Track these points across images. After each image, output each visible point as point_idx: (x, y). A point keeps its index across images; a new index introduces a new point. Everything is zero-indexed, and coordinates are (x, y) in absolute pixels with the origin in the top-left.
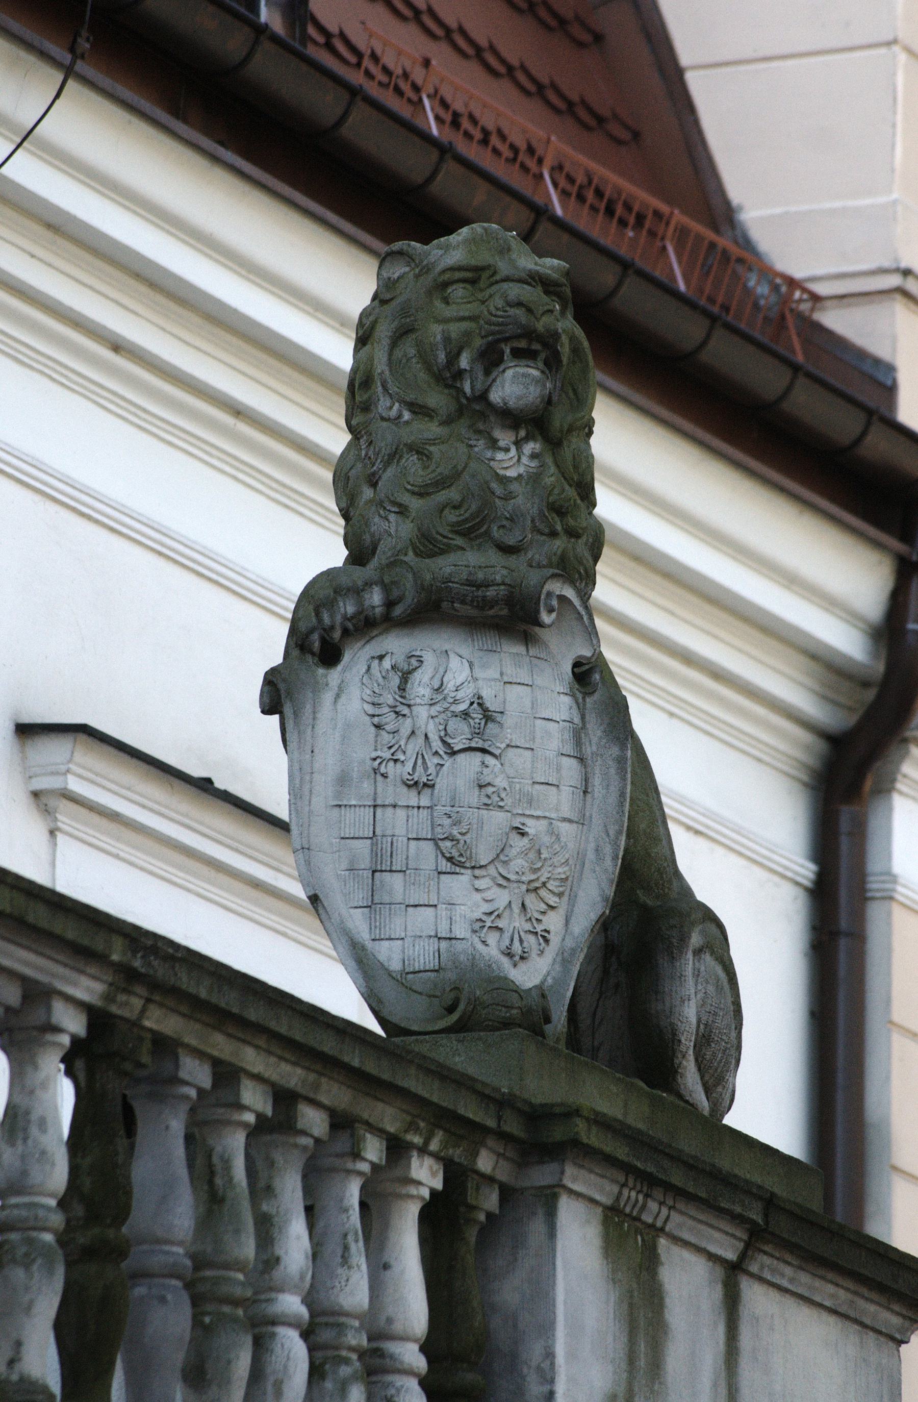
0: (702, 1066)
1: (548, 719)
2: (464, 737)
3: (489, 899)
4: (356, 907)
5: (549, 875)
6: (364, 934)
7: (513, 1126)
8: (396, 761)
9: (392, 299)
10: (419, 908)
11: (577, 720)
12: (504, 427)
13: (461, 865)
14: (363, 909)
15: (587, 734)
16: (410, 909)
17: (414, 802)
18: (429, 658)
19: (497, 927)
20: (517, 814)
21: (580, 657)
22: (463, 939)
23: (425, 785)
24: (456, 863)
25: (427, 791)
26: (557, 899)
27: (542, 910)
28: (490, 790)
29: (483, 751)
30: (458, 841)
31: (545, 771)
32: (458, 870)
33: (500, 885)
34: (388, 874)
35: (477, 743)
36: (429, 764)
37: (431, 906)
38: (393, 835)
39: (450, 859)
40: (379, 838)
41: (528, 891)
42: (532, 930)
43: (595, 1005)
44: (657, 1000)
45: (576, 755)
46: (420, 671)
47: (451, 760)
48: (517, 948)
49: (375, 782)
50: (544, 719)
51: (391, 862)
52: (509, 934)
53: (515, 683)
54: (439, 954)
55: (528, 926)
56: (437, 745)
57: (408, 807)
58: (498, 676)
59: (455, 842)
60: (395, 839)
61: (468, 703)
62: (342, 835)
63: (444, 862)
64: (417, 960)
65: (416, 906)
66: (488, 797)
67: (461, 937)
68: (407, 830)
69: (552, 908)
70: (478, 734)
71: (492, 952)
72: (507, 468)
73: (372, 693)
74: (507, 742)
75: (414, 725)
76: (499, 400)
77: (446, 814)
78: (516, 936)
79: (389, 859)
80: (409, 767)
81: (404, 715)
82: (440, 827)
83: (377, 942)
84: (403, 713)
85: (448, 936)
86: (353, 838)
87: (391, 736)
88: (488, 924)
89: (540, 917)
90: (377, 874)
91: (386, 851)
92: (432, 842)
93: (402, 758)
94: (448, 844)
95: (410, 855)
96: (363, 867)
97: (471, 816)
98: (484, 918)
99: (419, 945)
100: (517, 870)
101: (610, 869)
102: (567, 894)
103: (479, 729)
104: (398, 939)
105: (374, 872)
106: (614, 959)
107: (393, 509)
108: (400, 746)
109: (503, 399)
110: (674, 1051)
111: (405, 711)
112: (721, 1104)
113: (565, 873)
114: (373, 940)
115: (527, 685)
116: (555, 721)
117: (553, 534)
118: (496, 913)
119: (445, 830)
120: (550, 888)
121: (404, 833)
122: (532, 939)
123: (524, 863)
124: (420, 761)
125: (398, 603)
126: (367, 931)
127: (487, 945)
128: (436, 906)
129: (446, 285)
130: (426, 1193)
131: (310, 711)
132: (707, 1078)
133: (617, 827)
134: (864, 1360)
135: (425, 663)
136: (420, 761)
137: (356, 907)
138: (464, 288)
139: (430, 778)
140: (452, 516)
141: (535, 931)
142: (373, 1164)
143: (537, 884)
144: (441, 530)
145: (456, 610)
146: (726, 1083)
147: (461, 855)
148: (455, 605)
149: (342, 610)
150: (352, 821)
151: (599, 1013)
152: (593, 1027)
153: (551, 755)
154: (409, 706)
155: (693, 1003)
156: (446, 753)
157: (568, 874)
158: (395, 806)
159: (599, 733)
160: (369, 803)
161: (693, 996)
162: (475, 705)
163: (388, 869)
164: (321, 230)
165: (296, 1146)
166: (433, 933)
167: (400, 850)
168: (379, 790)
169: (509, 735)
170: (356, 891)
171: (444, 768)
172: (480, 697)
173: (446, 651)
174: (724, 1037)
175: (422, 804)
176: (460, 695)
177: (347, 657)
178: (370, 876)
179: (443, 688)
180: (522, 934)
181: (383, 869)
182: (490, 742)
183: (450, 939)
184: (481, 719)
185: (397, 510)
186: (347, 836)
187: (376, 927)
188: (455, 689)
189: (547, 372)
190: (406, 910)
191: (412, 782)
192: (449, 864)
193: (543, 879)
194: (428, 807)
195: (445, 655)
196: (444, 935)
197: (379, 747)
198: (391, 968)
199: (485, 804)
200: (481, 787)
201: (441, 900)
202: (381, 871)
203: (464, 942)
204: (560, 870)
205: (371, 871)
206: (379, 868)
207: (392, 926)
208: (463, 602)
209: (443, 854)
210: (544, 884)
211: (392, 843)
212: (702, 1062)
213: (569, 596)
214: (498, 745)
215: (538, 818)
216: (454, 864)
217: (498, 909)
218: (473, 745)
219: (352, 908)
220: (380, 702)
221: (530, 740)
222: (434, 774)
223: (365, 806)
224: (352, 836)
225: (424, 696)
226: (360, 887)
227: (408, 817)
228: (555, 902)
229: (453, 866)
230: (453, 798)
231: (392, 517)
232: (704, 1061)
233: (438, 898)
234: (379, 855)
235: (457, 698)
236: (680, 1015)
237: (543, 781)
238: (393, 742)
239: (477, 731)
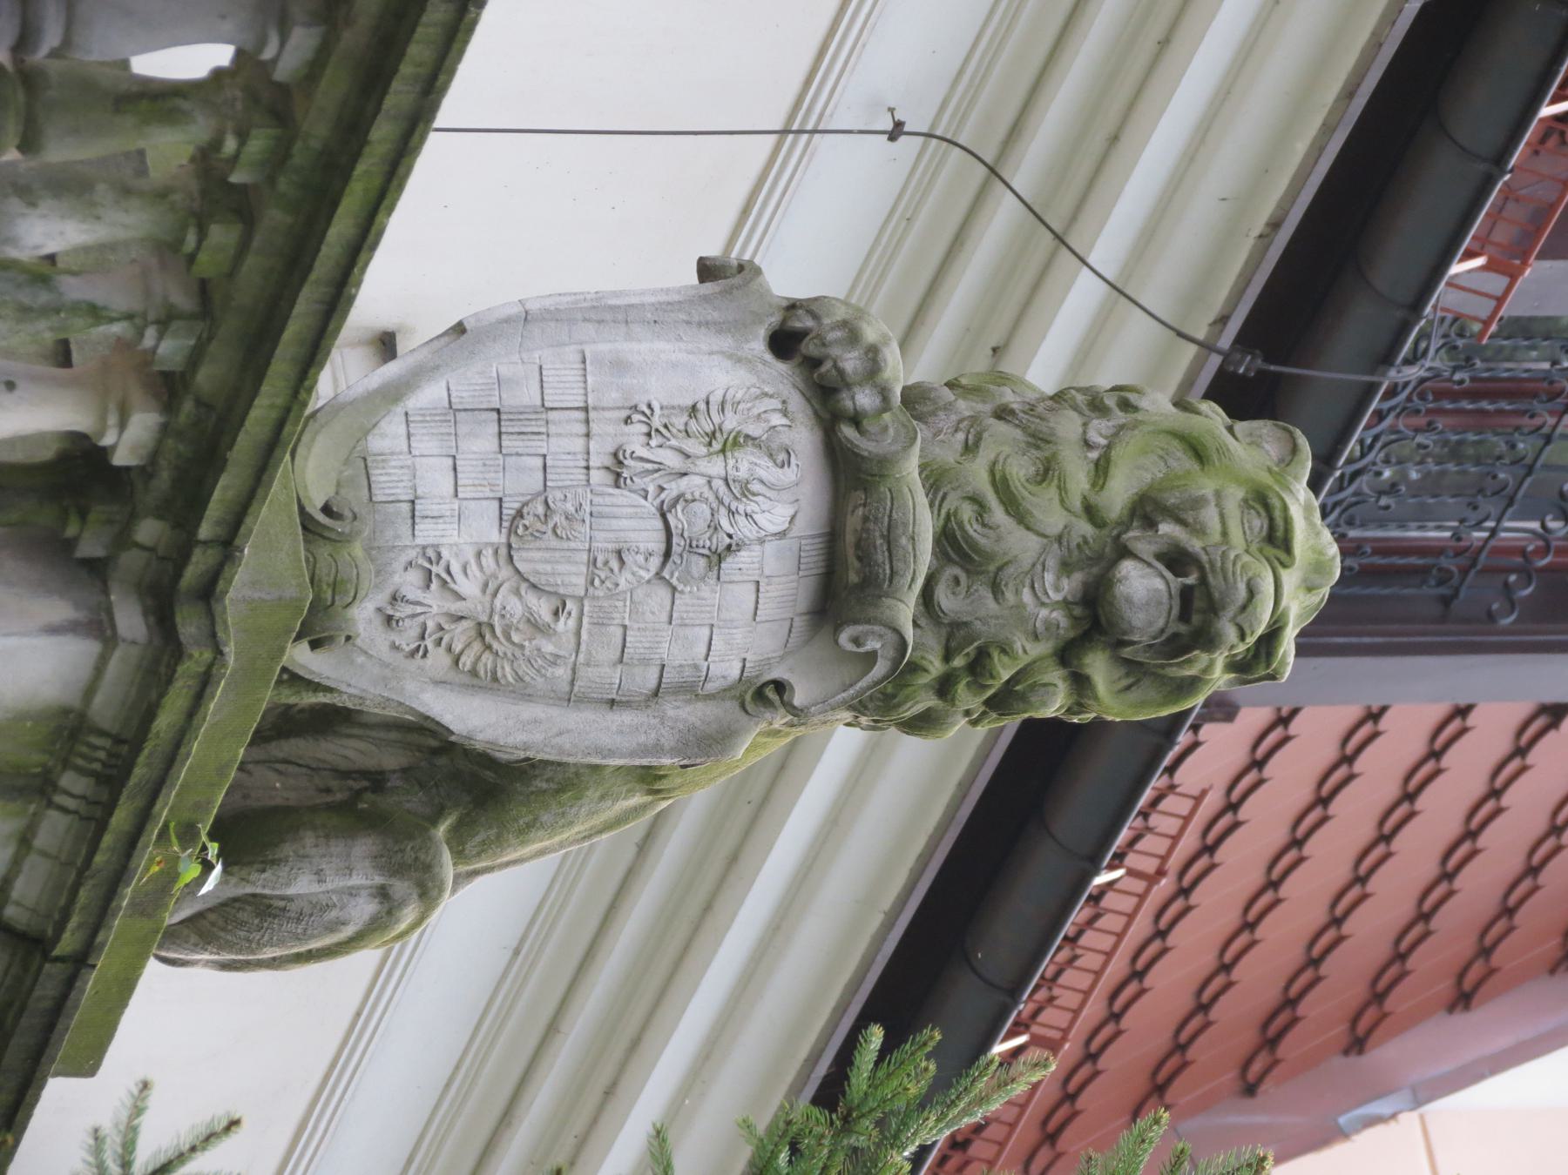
0: (228, 909)
1: (710, 644)
2: (686, 526)
3: (469, 571)
4: (449, 390)
5: (500, 654)
6: (415, 402)
8: (649, 435)
9: (1236, 439)
10: (452, 473)
11: (711, 687)
12: (1086, 585)
13: (512, 530)
14: (447, 399)
15: (688, 702)
16: (450, 461)
17: (595, 462)
18: (789, 475)
19: (430, 580)
20: (583, 605)
21: (792, 689)
22: (414, 535)
23: (618, 475)
24: (516, 522)
25: (610, 478)
26: (468, 667)
27: (453, 646)
28: (615, 564)
29: (667, 554)
30: (546, 522)
31: (641, 642)
32: (506, 524)
33: (486, 585)
34: (496, 429)
35: (679, 545)
36: (647, 480)
37: (456, 491)
38: (548, 435)
39: (520, 514)
40: (544, 416)
41: (480, 624)
42: (427, 633)
43: (301, 762)
44: (318, 837)
45: (663, 686)
46: (770, 464)
47: (653, 510)
48: (403, 611)
49: (619, 408)
50: (711, 639)
51: (512, 433)
52: (421, 600)
53: (758, 597)
54: (392, 502)
55: (431, 625)
57: (588, 453)
58: (767, 572)
59: (542, 518)
60: (544, 437)
61: (731, 531)
62: (544, 367)
63: (517, 505)
64: (383, 471)
65: (455, 469)
66: (606, 563)
67: (416, 533)
68: (557, 453)
69: (457, 662)
70: (691, 546)
71: (398, 575)
72: (1033, 587)
73: (736, 400)
74: (680, 587)
75: (698, 457)
76: (1124, 572)
77: (581, 505)
78: (419, 609)
79: (516, 429)
80: (642, 452)
81: (710, 444)
82: (563, 498)
83: (404, 418)
84: (714, 442)
85: (417, 513)
86: (542, 380)
87: (682, 428)
88: (434, 569)
89: (444, 643)
90: (494, 415)
91: (525, 426)
92: (542, 488)
93: (653, 443)
94: (540, 510)
95: (524, 458)
96: (504, 396)
98: (443, 563)
99: (403, 474)
100: (508, 608)
101: (510, 740)
102: (475, 681)
103: (697, 546)
104: (410, 446)
105: (498, 411)
106: (365, 783)
107: (970, 437)
108: (669, 440)
109: (1126, 578)
110: (251, 863)
111: (717, 446)
112: (174, 943)
113: (504, 676)
114: (406, 414)
115: (755, 614)
116: (708, 655)
117: (947, 658)
118: (448, 579)
119: (559, 504)
120: (483, 657)
121: (553, 449)
122: (415, 632)
123: (517, 617)
124: (649, 466)
125: (859, 432)
126: (419, 405)
127: (406, 569)
128: (456, 496)
130: (108, 440)
131: (709, 318)
132: (212, 917)
133: (568, 746)
135: (778, 469)
136: (649, 466)
137: (449, 390)
138: (1262, 527)
139: (628, 481)
140: (967, 512)
141: (426, 636)
142: (154, 350)
143: (488, 637)
144: (949, 498)
145: (853, 511)
146: (202, 948)
147: (526, 527)
148: (861, 509)
149: (849, 356)
150: (564, 379)
151: (291, 768)
152: (270, 762)
153: (662, 651)
154: (723, 451)
155: (316, 888)
156: (663, 502)
157: (503, 682)
158: (588, 435)
159: (692, 719)
160: (590, 401)
161: (324, 887)
162: (728, 541)
163: (503, 430)
165: (184, 228)
166: (419, 492)
167: (529, 443)
168: (608, 414)
169: (689, 589)
170: (471, 388)
171: (643, 502)
172: (739, 547)
173: (712, 625)
174: (266, 938)
175: (592, 472)
176: (741, 520)
177: (781, 367)
178: (493, 406)
179: (750, 497)
180: (421, 618)
181: (503, 423)
182: (679, 562)
183: (413, 517)
184: (710, 549)
185: (970, 442)
186: (544, 373)
187: (423, 415)
188: (749, 511)
189: (1164, 637)
190: (449, 456)
191: (621, 457)
192: (513, 512)
193: (495, 645)
194: (588, 481)
195: (793, 499)
196: (418, 507)
197: (666, 412)
198: (370, 438)
199: (595, 560)
200: (619, 553)
201: (465, 503)
202: (499, 420)
203: (411, 537)
204: (508, 669)
205: (498, 406)
206: (504, 417)
207: (427, 438)
208: (866, 519)
209: (526, 504)
210: (489, 647)
211: (539, 433)
212: (234, 908)
213: (875, 669)
214: (676, 574)
215: (578, 634)
216: (514, 518)
217: (455, 582)
218: (675, 540)
219: (448, 383)
220: (726, 412)
221: (682, 618)
222: (634, 487)
223: (586, 395)
224: (545, 379)
225: (737, 470)
226: (477, 394)
227: (574, 454)
228: (464, 665)
229: (510, 518)
230: (601, 516)
231: (961, 436)
232: (234, 911)
233: (466, 499)
234: (521, 417)
235: (736, 515)
236: (299, 869)
237: (628, 639)
238: (674, 431)
239: (694, 544)
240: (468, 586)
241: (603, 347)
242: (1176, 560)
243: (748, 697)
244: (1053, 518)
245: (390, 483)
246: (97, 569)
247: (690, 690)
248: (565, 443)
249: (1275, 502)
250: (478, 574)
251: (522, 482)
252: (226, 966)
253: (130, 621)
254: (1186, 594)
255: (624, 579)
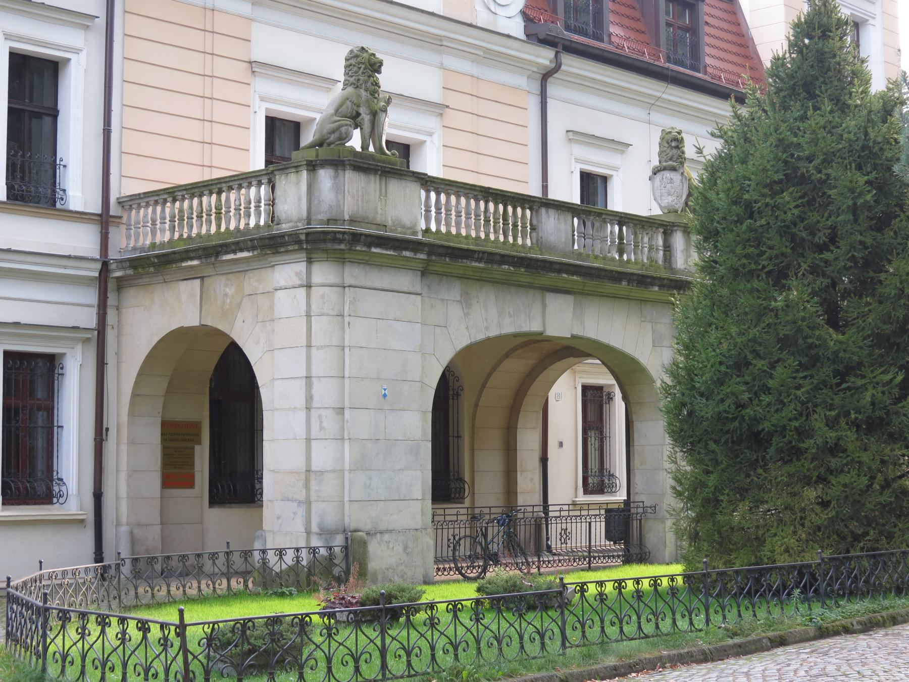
242: (672, 141)
244: (668, 151)
245: (666, 205)
246: (672, 231)
247: (682, 180)
248: (663, 191)
251: (666, 194)
253: (675, 228)
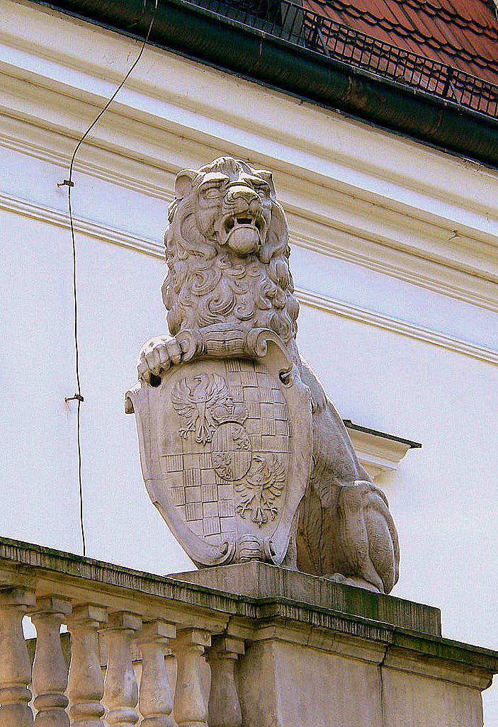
7: (247, 611)
56: (211, 422)
94: (220, 470)
97: (232, 454)
124: (203, 431)
129: (204, 191)
134: (460, 700)
136: (203, 431)
162: (229, 400)
164: (409, 147)
168: (184, 446)
240: (250, 494)
241: (161, 450)
243: (286, 386)
248: (194, 463)
249: (205, 187)
250: (245, 491)
252: (397, 558)
254: (241, 221)
255: (244, 436)
